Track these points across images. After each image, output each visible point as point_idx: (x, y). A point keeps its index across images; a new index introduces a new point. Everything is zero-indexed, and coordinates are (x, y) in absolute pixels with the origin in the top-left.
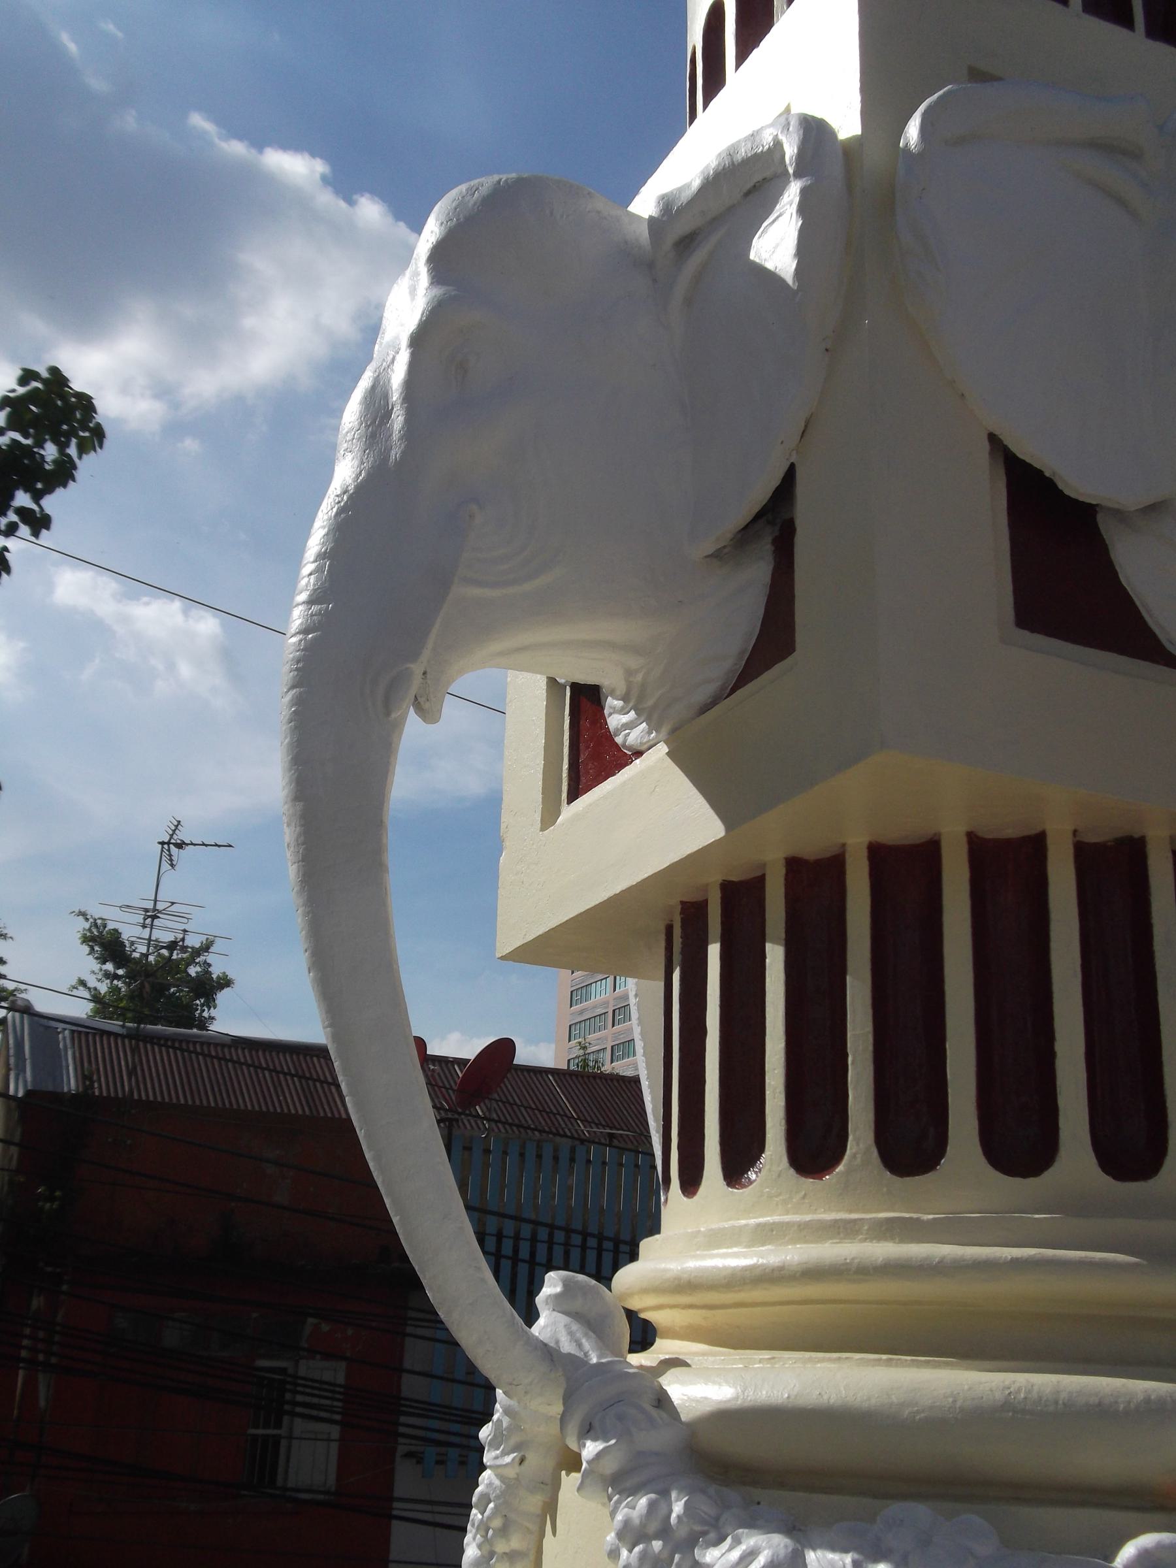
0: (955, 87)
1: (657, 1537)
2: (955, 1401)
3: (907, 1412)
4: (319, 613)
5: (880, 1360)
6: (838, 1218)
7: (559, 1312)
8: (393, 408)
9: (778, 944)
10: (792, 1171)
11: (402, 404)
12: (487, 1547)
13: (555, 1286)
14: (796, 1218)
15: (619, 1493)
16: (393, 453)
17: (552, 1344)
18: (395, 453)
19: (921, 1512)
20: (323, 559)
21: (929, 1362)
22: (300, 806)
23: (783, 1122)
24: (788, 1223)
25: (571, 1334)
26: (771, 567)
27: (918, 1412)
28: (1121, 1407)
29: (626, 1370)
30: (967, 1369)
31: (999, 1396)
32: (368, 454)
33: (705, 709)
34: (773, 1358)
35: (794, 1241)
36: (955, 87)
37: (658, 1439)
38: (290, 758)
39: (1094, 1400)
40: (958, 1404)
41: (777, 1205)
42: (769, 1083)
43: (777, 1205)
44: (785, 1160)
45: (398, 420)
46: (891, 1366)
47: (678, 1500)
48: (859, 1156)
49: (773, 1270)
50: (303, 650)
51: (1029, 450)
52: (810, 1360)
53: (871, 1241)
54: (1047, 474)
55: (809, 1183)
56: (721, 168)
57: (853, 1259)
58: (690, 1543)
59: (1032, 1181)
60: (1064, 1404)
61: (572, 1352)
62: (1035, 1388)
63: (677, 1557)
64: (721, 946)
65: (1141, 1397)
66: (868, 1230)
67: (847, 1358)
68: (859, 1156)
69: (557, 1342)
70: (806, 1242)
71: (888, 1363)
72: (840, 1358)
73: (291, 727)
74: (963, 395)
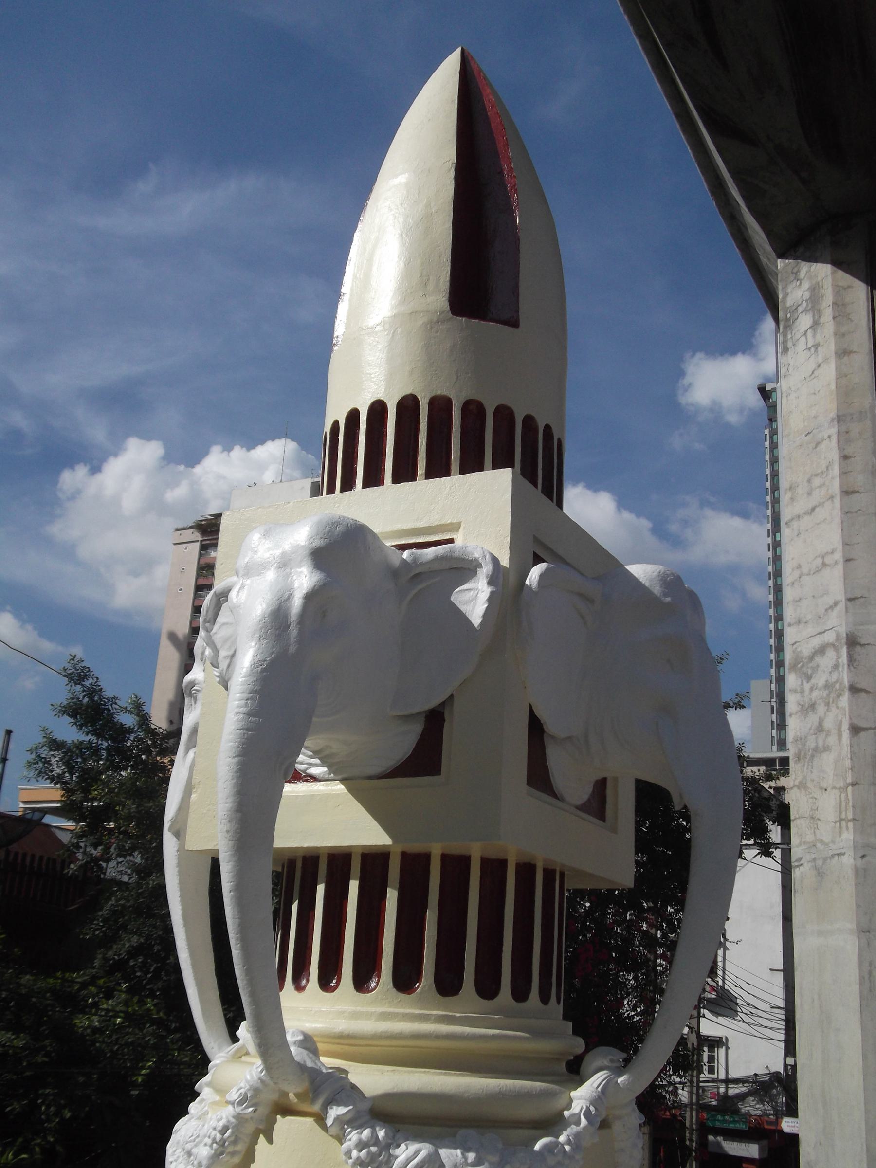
0: (555, 566)
1: (373, 1145)
2: (483, 1091)
3: (466, 1096)
4: (255, 722)
5: (442, 1073)
6: (421, 1013)
7: (302, 1048)
8: (290, 624)
9: (395, 889)
10: (394, 989)
11: (297, 624)
12: (221, 1149)
13: (298, 1036)
14: (402, 1010)
15: (352, 1128)
16: (291, 648)
17: (302, 1063)
18: (292, 649)
19: (472, 1132)
20: (255, 693)
21: (446, 1073)
22: (239, 815)
23: (392, 968)
24: (397, 1013)
25: (310, 1058)
26: (423, 727)
27: (470, 1095)
28: (534, 1093)
29: (341, 1075)
30: (475, 1077)
31: (497, 1089)
32: (276, 644)
33: (370, 778)
34: (394, 1070)
35: (400, 1021)
36: (555, 566)
37: (366, 1106)
38: (235, 790)
39: (526, 1090)
40: (484, 1092)
41: (385, 1003)
42: (385, 950)
43: (385, 1003)
44: (391, 984)
45: (293, 632)
46: (446, 1075)
47: (380, 1130)
48: (427, 987)
49: (397, 1034)
50: (246, 739)
51: (539, 713)
52: (412, 1072)
53: (435, 1024)
54: (542, 722)
55: (402, 996)
56: (445, 555)
57: (434, 1031)
58: (387, 1147)
59: (491, 1001)
60: (518, 1092)
61: (314, 1067)
62: (508, 1086)
63: (383, 1153)
64: (359, 882)
65: (539, 1089)
66: (434, 1019)
67: (428, 1072)
68: (427, 987)
69: (305, 1062)
70: (406, 1022)
71: (445, 1074)
72: (425, 1072)
73: (237, 775)
74: (525, 687)
